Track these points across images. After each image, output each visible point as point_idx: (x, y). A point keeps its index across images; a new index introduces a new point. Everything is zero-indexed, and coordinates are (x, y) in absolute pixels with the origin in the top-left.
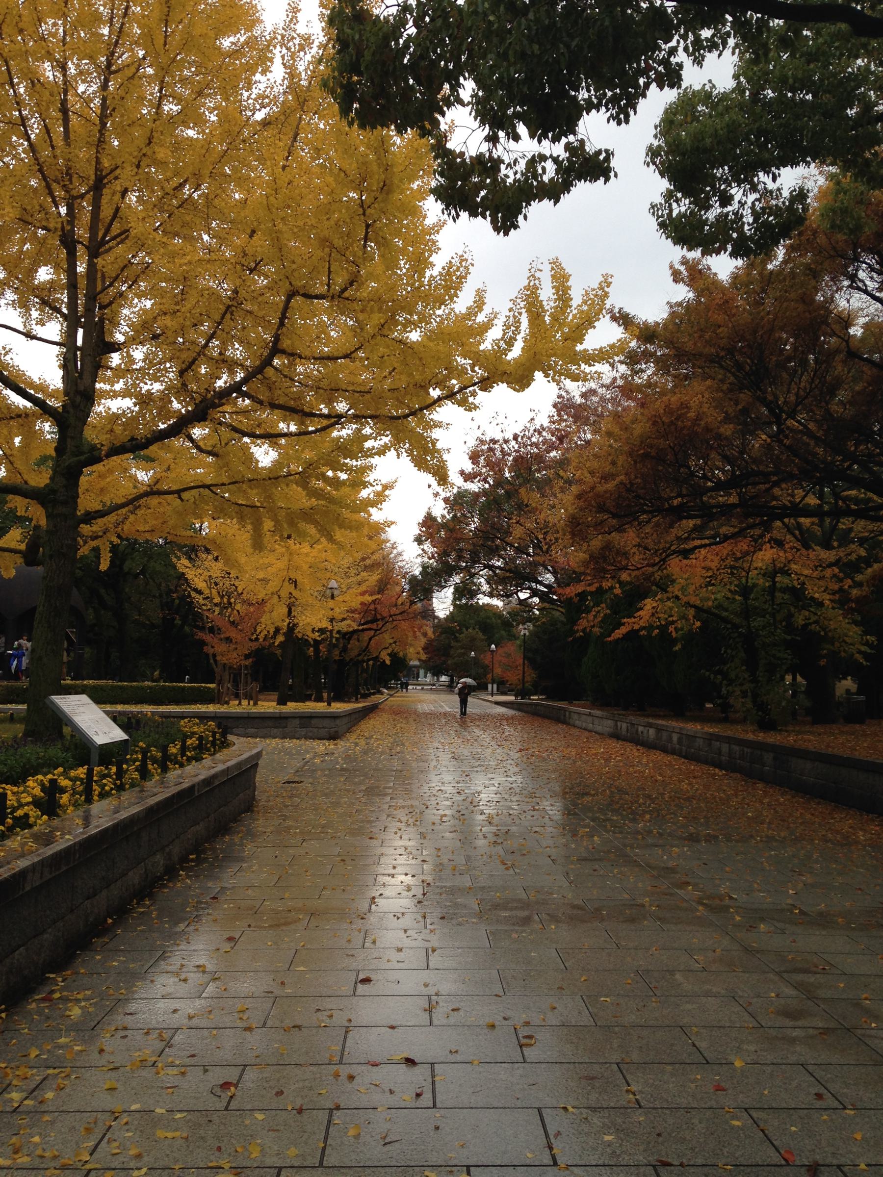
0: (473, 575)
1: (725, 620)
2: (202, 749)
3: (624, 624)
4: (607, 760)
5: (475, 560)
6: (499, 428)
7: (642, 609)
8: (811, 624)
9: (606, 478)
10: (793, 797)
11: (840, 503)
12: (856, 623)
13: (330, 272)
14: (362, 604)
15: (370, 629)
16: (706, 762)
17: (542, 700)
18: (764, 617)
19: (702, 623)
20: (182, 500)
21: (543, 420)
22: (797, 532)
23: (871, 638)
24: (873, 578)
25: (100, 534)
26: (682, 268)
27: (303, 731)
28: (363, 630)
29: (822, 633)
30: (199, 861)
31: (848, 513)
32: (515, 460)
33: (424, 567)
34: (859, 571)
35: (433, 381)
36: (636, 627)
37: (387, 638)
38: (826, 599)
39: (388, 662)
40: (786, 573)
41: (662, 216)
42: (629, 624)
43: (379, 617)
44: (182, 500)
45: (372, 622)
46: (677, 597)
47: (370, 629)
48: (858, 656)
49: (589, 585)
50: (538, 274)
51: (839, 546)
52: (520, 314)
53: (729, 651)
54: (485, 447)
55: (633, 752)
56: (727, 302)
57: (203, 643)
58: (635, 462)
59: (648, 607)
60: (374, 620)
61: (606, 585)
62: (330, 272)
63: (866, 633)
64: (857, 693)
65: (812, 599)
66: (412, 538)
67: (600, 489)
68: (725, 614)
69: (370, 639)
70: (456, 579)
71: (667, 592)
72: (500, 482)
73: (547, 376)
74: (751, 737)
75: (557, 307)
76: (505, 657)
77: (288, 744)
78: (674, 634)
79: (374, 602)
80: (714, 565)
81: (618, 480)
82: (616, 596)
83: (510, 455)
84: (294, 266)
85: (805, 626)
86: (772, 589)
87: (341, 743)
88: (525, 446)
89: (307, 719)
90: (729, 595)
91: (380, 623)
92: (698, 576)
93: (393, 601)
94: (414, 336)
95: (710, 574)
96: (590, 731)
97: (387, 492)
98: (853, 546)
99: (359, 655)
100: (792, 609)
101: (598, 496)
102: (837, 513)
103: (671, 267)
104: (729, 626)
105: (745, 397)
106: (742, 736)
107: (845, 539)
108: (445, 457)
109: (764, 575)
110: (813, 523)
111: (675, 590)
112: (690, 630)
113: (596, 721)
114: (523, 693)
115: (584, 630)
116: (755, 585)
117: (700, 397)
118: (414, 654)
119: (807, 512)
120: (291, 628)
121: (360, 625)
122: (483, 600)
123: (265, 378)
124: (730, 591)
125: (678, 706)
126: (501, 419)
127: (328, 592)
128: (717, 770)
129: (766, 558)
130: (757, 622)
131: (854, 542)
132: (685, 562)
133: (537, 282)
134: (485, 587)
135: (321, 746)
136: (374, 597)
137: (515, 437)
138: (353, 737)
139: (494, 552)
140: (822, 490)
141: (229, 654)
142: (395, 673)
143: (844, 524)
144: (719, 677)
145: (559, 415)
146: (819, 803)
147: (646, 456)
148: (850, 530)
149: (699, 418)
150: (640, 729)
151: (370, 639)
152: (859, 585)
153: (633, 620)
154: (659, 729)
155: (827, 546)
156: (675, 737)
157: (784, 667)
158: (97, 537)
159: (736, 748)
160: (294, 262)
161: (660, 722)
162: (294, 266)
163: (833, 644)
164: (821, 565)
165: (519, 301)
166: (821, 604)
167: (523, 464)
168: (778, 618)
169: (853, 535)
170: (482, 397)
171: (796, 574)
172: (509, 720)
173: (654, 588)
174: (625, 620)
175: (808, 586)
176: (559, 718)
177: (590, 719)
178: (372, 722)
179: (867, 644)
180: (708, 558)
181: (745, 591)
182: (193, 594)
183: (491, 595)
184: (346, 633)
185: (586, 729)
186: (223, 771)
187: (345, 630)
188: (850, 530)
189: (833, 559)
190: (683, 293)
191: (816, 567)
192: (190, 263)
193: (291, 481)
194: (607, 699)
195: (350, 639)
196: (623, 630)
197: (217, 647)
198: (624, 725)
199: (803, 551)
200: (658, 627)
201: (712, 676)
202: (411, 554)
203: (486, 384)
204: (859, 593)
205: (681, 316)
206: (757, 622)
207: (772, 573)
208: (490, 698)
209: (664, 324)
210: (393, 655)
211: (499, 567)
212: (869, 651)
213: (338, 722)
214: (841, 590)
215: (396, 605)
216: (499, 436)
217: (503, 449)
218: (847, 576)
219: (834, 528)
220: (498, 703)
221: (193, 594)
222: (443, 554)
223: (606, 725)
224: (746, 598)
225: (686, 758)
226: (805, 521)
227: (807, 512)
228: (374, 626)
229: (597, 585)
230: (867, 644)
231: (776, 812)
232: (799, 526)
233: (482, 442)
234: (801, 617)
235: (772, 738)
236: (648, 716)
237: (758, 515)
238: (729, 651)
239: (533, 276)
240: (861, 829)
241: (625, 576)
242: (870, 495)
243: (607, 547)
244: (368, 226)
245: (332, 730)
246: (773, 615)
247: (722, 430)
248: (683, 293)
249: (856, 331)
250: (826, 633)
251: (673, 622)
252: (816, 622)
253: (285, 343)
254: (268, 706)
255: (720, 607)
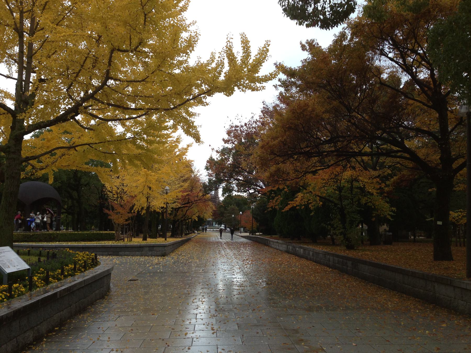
0: (230, 183)
1: (332, 202)
2: (86, 267)
3: (289, 204)
4: (281, 265)
5: (231, 176)
6: (239, 121)
7: (297, 197)
8: (368, 203)
9: (274, 138)
10: (360, 282)
11: (380, 151)
12: (387, 202)
13: (130, 39)
14: (182, 196)
15: (187, 207)
16: (324, 265)
17: (260, 235)
18: (348, 200)
19: (323, 202)
20: (77, 151)
21: (257, 117)
22: (362, 164)
23: (394, 209)
24: (394, 183)
25: (44, 167)
26: (306, 45)
27: (150, 253)
28: (183, 207)
29: (373, 207)
30: (60, 330)
31: (382, 154)
32: (246, 134)
33: (210, 180)
34: (388, 179)
35: (184, 91)
36: (295, 205)
37: (195, 210)
38: (374, 192)
39: (197, 220)
40: (357, 180)
41: (285, 5)
42: (292, 204)
43: (190, 201)
44: (77, 151)
45: (187, 203)
46: (311, 192)
47: (187, 207)
48: (388, 216)
49: (274, 187)
50: (231, 40)
51: (380, 169)
52: (224, 59)
53: (333, 215)
54: (234, 129)
55: (293, 259)
56: (325, 58)
57: (108, 215)
58: (285, 131)
59: (300, 196)
60: (188, 203)
61: (281, 187)
62: (130, 39)
63: (391, 206)
64: (389, 231)
65: (369, 192)
66: (204, 168)
67: (271, 144)
68: (331, 199)
69: (187, 211)
70: (224, 185)
71: (306, 190)
72: (240, 143)
73: (239, 88)
74: (342, 254)
75: (243, 56)
76: (245, 216)
77: (142, 259)
78: (312, 208)
79: (188, 195)
80: (326, 178)
81: (279, 139)
82: (286, 192)
83: (244, 132)
84: (112, 36)
85: (366, 204)
86: (352, 188)
87: (166, 258)
88: (250, 128)
89: (151, 247)
90: (333, 191)
91: (191, 204)
92: (319, 183)
93: (194, 193)
94: (177, 71)
95: (325, 182)
96: (277, 249)
97: (189, 148)
98: (385, 169)
99: (182, 217)
100: (360, 196)
101: (270, 147)
102: (379, 155)
103: (301, 43)
104: (333, 204)
105: (335, 103)
106: (339, 253)
107: (382, 166)
108: (198, 129)
109: (348, 182)
110: (369, 160)
111: (310, 189)
112: (318, 206)
113: (280, 245)
114: (253, 232)
115: (272, 207)
116: (344, 186)
117: (311, 98)
118: (208, 217)
119: (366, 154)
120: (148, 208)
121: (182, 205)
122: (234, 193)
123: (104, 91)
124: (333, 189)
125: (314, 238)
126: (240, 117)
127: (165, 191)
128: (328, 268)
129: (348, 175)
130: (345, 202)
131: (386, 167)
132: (314, 177)
133: (231, 44)
134: (236, 188)
135: (155, 260)
136: (187, 193)
137: (246, 124)
138: (173, 255)
139: (239, 173)
140: (372, 146)
141: (119, 218)
142: (200, 224)
143: (381, 160)
144: (329, 226)
145: (264, 115)
146: (371, 286)
147: (290, 128)
148: (384, 162)
149: (313, 110)
150: (297, 249)
151: (187, 211)
152: (387, 186)
153: (293, 202)
154: (305, 249)
155: (375, 169)
156: (311, 253)
157: (357, 222)
158: (43, 169)
159: (336, 259)
160: (112, 34)
161: (305, 246)
162: (112, 36)
163: (378, 211)
164: (371, 178)
165: (223, 53)
166: (372, 194)
167: (249, 136)
168: (354, 200)
169: (385, 164)
170: (209, 99)
171: (361, 181)
172: (244, 244)
173: (301, 188)
174: (290, 202)
175: (366, 186)
176: (265, 243)
177: (277, 244)
178: (185, 247)
179: (392, 211)
180: (324, 175)
181: (340, 189)
182: (108, 193)
183: (238, 191)
184: (176, 209)
185: (276, 249)
186: (81, 282)
187: (175, 207)
188: (384, 162)
189: (377, 175)
190: (306, 55)
191: (370, 178)
192: (64, 36)
193: (128, 141)
194: (284, 235)
195: (177, 211)
196: (289, 207)
197: (114, 217)
198: (291, 247)
199: (364, 171)
200: (304, 205)
201: (326, 226)
202: (204, 176)
203: (209, 93)
204: (388, 189)
205: (307, 65)
206: (345, 202)
207: (353, 180)
208: (240, 234)
209: (299, 70)
210: (199, 217)
211: (241, 180)
212: (393, 214)
213: (166, 248)
214: (380, 188)
215: (197, 196)
216: (239, 124)
217: (241, 130)
218: (383, 181)
219: (377, 162)
220: (242, 237)
221: (108, 193)
222: (217, 175)
223: (284, 247)
224: (340, 191)
225: (315, 262)
226: (365, 158)
227: (366, 154)
228: (188, 205)
229: (277, 187)
230: (392, 211)
231: (351, 291)
232: (363, 161)
233: (232, 127)
234: (364, 200)
235: (350, 254)
236: (300, 243)
237: (344, 155)
238: (333, 215)
239: (229, 41)
240: (390, 301)
241: (288, 183)
242: (392, 147)
243: (278, 170)
244: (145, 15)
245: (163, 252)
246: (352, 199)
247: (324, 116)
248: (306, 55)
249: (385, 76)
250: (374, 207)
251: (311, 203)
252: (370, 202)
253: (112, 74)
254: (137, 241)
255: (329, 196)
